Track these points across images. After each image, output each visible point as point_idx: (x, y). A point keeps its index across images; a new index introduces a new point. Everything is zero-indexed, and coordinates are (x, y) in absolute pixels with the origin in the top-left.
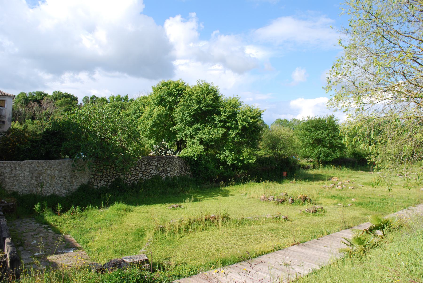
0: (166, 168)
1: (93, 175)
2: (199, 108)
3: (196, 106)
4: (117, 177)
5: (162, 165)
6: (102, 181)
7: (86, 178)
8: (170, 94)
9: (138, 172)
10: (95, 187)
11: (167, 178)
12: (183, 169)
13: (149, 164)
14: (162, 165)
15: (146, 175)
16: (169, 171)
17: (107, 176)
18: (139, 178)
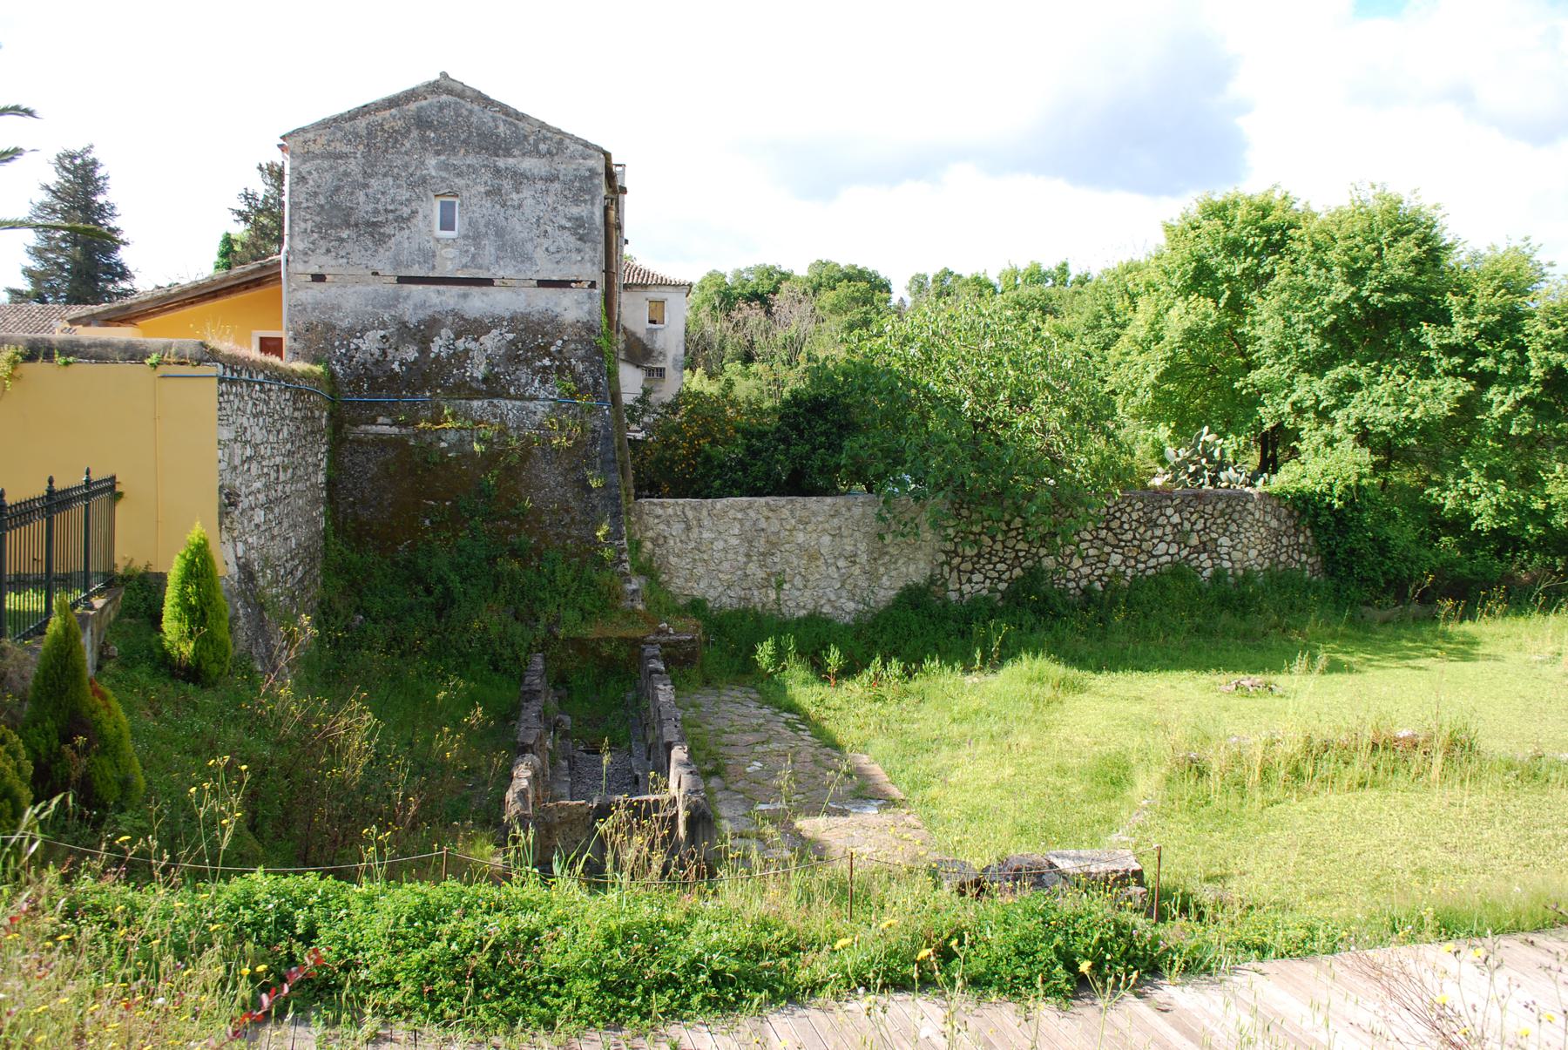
0: (1214, 535)
1: (946, 553)
2: (1355, 297)
3: (1342, 291)
4: (1030, 563)
5: (1199, 526)
6: (977, 577)
7: (922, 565)
8: (1234, 248)
9: (1107, 549)
10: (953, 596)
11: (1219, 575)
12: (1285, 541)
13: (1150, 520)
14: (1199, 526)
15: (1137, 561)
16: (1225, 550)
17: (995, 559)
18: (1109, 571)
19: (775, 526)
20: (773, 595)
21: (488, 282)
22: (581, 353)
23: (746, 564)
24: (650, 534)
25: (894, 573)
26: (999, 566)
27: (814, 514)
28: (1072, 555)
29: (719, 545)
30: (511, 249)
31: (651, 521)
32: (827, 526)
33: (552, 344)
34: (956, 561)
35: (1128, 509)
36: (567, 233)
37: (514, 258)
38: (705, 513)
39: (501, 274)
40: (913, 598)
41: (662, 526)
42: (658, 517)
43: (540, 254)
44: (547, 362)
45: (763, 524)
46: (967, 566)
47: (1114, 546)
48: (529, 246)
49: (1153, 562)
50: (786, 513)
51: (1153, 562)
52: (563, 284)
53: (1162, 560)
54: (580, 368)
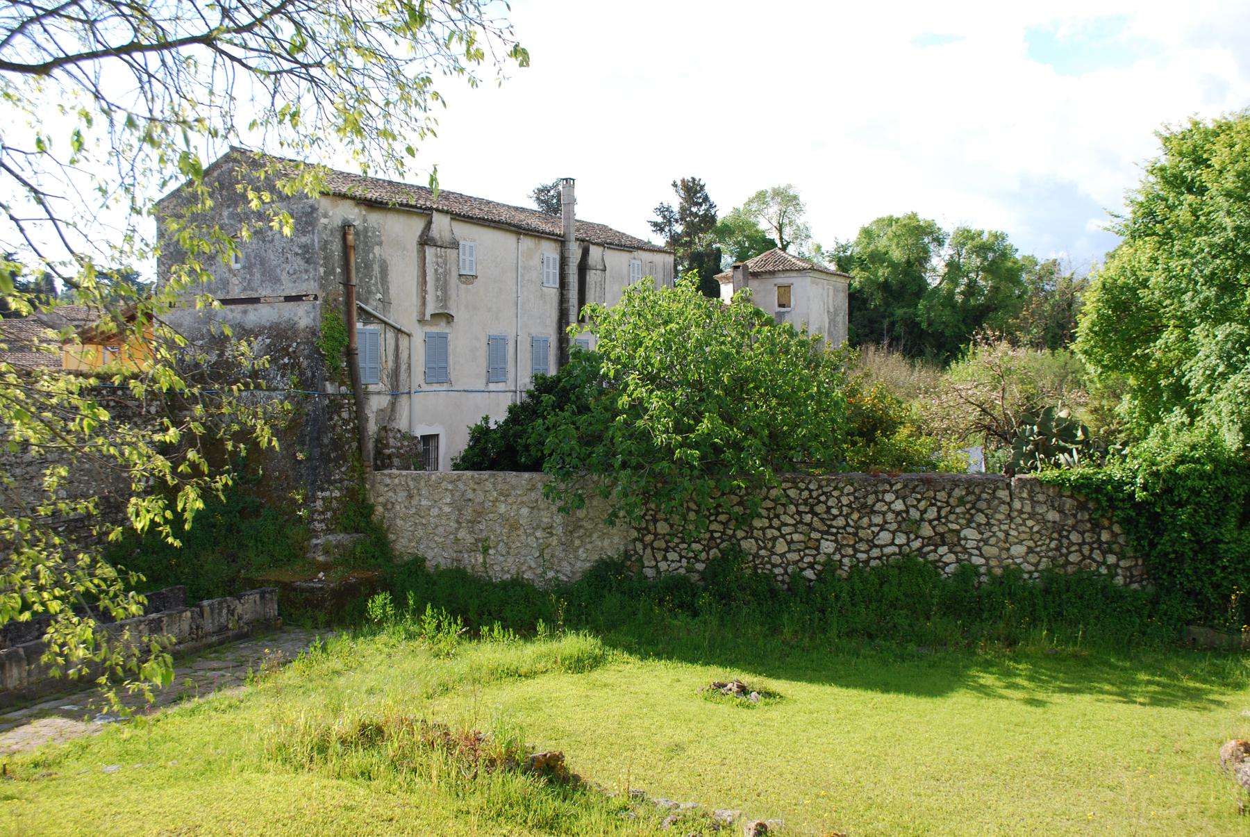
1: (638, 530)
6: (672, 556)
7: (616, 540)
9: (814, 535)
10: (650, 573)
11: (967, 573)
13: (864, 506)
14: (932, 513)
19: (480, 497)
20: (481, 559)
21: (255, 301)
22: (306, 352)
23: (457, 529)
24: (381, 499)
25: (589, 546)
26: (694, 546)
27: (513, 488)
28: (774, 539)
29: (435, 512)
30: (271, 276)
31: (383, 489)
32: (525, 499)
33: (290, 346)
34: (649, 538)
35: (835, 493)
36: (299, 258)
37: (270, 281)
38: (422, 483)
39: (264, 293)
40: (605, 575)
41: (390, 494)
42: (387, 485)
43: (284, 277)
44: (286, 360)
45: (470, 495)
46: (660, 544)
47: (823, 532)
48: (278, 270)
49: (875, 552)
50: (489, 486)
51: (875, 552)
52: (298, 298)
53: (888, 550)
54: (305, 364)
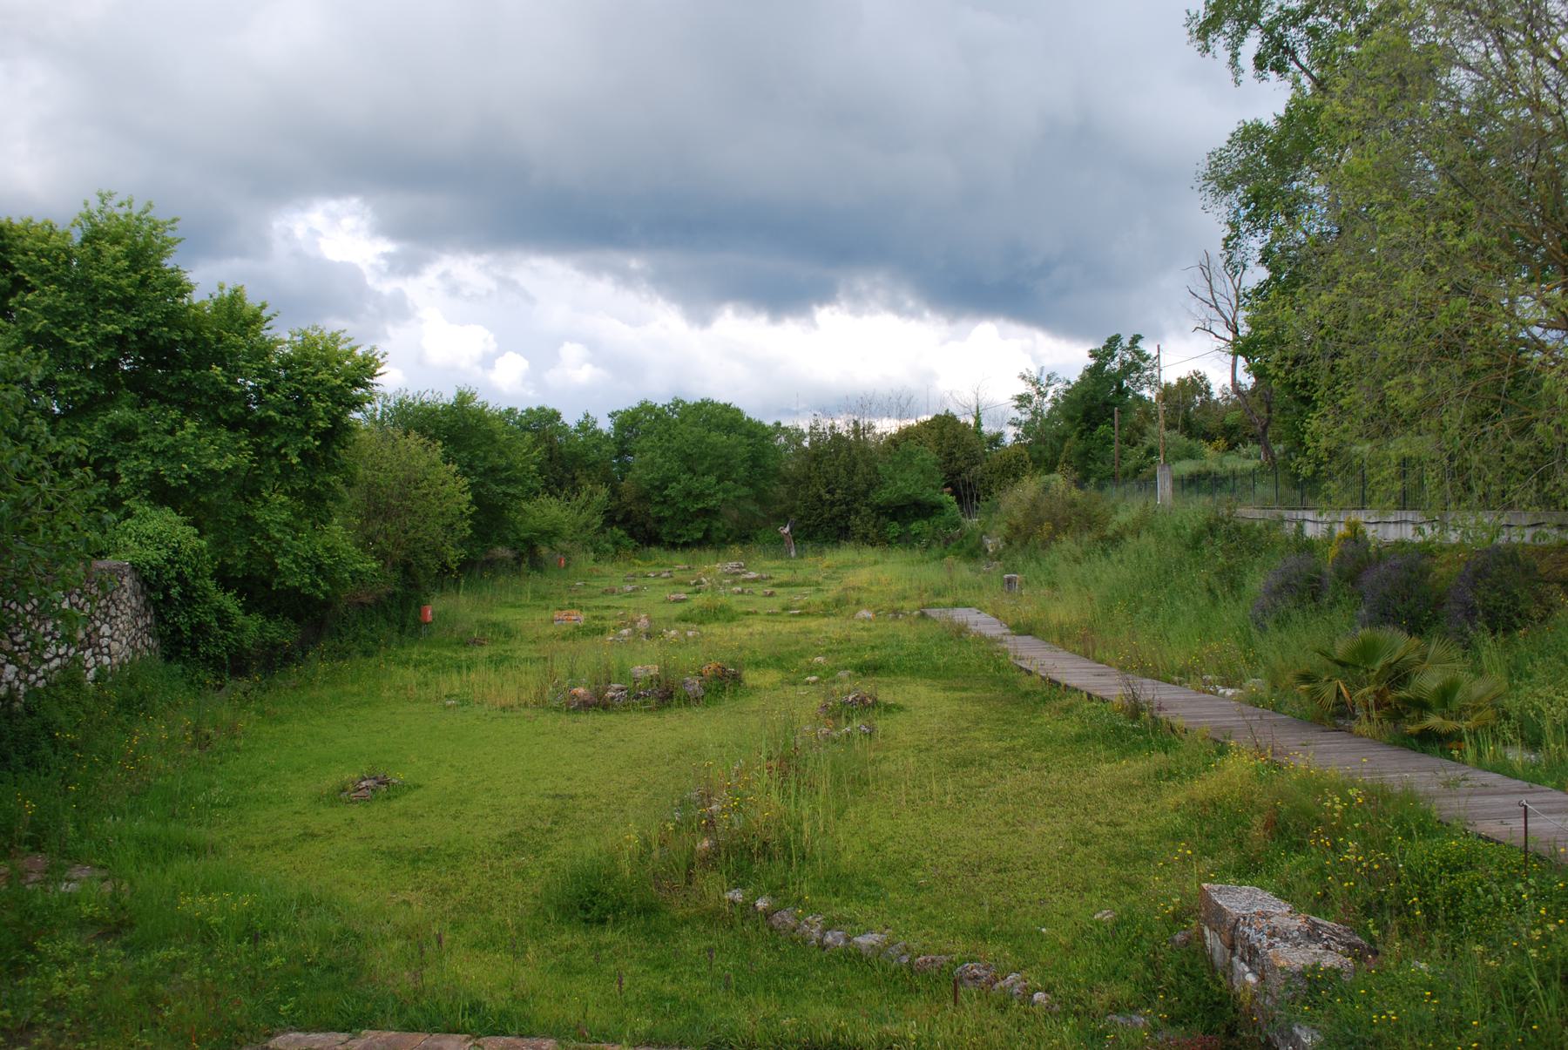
0: (98, 623)
